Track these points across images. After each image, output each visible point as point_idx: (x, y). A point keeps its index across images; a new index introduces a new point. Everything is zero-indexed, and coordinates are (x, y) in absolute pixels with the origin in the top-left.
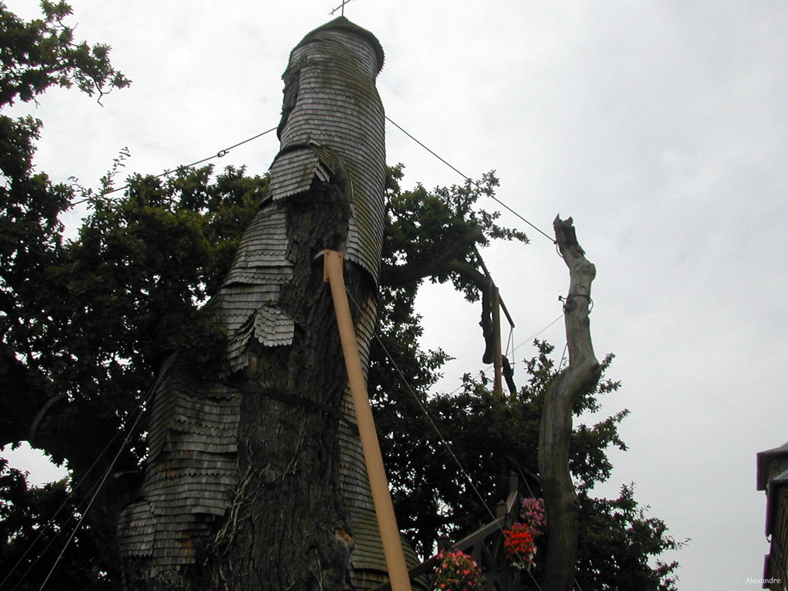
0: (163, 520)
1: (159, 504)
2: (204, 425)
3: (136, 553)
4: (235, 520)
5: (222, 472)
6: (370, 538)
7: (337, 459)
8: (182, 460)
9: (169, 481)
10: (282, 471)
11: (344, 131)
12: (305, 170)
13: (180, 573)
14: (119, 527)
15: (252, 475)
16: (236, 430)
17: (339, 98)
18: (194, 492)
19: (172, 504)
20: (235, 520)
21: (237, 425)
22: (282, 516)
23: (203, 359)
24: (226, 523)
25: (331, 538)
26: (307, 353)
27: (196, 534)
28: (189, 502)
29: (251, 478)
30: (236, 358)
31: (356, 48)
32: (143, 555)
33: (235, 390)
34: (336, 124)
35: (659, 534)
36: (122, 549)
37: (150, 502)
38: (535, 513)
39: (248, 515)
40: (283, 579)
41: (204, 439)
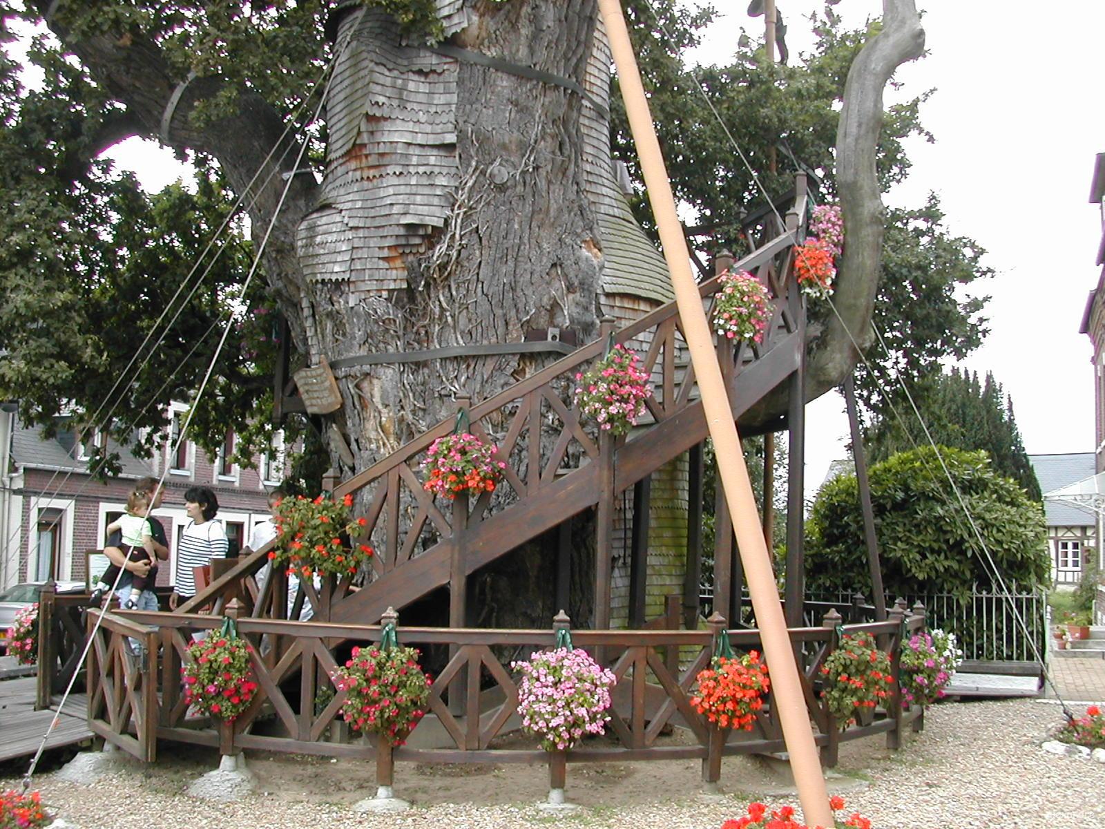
0: (361, 233)
1: (354, 213)
2: (409, 106)
3: (327, 277)
4: (458, 232)
5: (437, 170)
6: (621, 253)
7: (579, 152)
8: (382, 155)
9: (365, 183)
10: (515, 167)
13: (388, 300)
14: (300, 243)
15: (477, 174)
16: (452, 114)
18: (401, 197)
19: (373, 213)
20: (458, 232)
21: (453, 107)
22: (516, 226)
23: (405, 18)
24: (445, 235)
25: (578, 254)
26: (543, 9)
27: (407, 251)
28: (395, 209)
29: (477, 178)
30: (449, 17)
32: (337, 280)
33: (449, 60)
35: (975, 259)
36: (306, 271)
37: (341, 210)
38: (830, 225)
39: (474, 226)
40: (521, 306)
41: (410, 126)
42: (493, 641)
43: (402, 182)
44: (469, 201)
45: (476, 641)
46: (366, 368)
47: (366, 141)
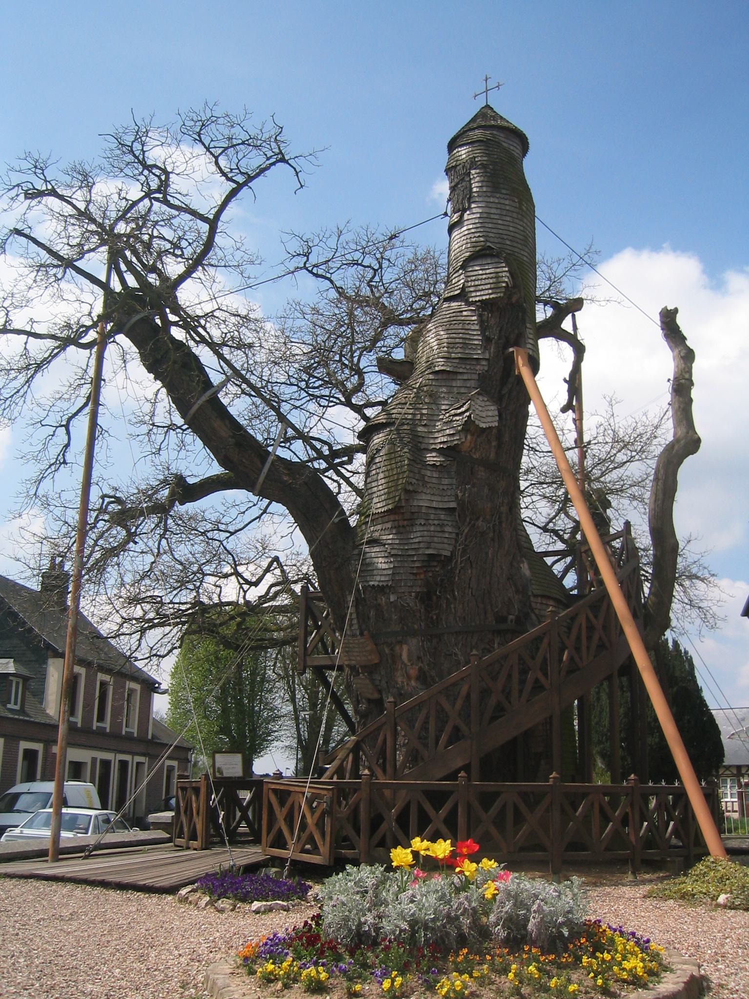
11: (512, 234)
12: (497, 277)
13: (416, 597)
17: (507, 202)
31: (512, 148)
34: (506, 228)
37: (385, 544)
41: (429, 497)
43: (425, 529)
44: (465, 541)
47: (404, 505)
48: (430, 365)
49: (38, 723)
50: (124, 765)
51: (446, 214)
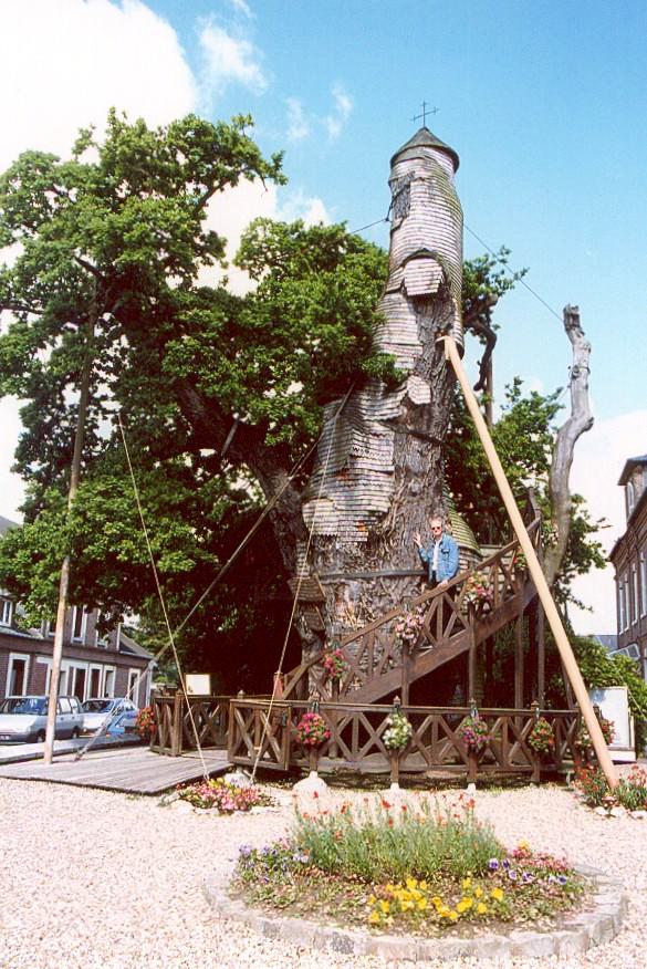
17: (441, 211)
19: (351, 503)
42: (444, 712)
45: (436, 712)
46: (343, 580)
48: (40, 465)
49: (34, 640)
50: (96, 673)
51: (387, 220)
